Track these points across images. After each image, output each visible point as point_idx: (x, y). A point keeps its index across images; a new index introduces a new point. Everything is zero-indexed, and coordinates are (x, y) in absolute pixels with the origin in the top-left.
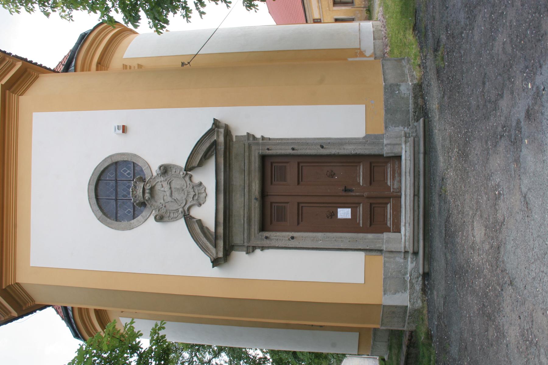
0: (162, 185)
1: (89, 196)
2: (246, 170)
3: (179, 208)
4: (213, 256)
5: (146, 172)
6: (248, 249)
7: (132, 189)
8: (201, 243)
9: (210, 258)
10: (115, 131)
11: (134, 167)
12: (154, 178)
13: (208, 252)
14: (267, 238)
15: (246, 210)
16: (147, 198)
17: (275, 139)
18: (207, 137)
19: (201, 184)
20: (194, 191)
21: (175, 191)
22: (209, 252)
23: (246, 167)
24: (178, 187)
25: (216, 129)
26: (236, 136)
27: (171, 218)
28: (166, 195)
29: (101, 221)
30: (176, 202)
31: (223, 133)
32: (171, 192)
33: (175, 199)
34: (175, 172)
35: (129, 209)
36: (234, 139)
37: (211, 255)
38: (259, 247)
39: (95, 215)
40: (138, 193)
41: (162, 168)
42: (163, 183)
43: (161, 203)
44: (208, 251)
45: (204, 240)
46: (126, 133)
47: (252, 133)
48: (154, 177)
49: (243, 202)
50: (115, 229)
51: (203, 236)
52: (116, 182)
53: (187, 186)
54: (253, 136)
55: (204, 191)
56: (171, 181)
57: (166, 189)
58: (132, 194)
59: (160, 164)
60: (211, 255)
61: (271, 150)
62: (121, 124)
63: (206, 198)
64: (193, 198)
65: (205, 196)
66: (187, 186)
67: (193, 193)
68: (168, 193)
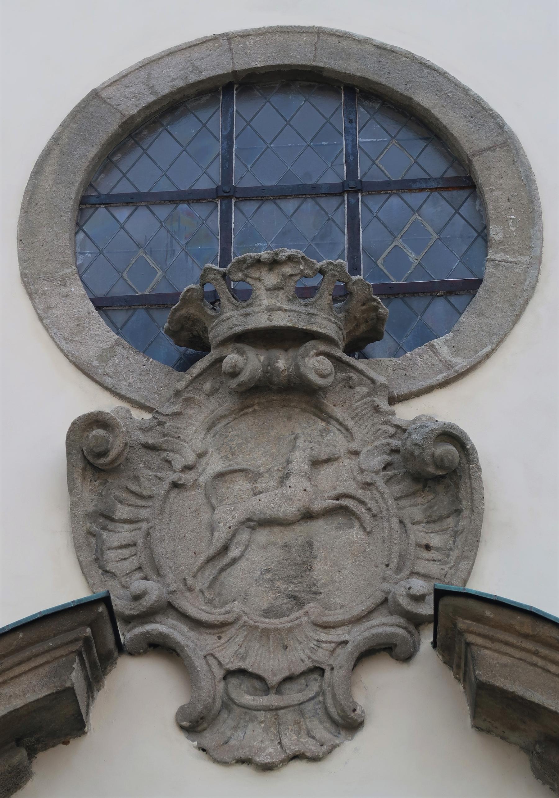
1: (245, 35)
12: (376, 409)
24: (317, 565)
33: (234, 552)
41: (451, 448)
48: (384, 405)
53: (326, 627)
64: (242, 672)
65: (261, 759)
66: (326, 627)
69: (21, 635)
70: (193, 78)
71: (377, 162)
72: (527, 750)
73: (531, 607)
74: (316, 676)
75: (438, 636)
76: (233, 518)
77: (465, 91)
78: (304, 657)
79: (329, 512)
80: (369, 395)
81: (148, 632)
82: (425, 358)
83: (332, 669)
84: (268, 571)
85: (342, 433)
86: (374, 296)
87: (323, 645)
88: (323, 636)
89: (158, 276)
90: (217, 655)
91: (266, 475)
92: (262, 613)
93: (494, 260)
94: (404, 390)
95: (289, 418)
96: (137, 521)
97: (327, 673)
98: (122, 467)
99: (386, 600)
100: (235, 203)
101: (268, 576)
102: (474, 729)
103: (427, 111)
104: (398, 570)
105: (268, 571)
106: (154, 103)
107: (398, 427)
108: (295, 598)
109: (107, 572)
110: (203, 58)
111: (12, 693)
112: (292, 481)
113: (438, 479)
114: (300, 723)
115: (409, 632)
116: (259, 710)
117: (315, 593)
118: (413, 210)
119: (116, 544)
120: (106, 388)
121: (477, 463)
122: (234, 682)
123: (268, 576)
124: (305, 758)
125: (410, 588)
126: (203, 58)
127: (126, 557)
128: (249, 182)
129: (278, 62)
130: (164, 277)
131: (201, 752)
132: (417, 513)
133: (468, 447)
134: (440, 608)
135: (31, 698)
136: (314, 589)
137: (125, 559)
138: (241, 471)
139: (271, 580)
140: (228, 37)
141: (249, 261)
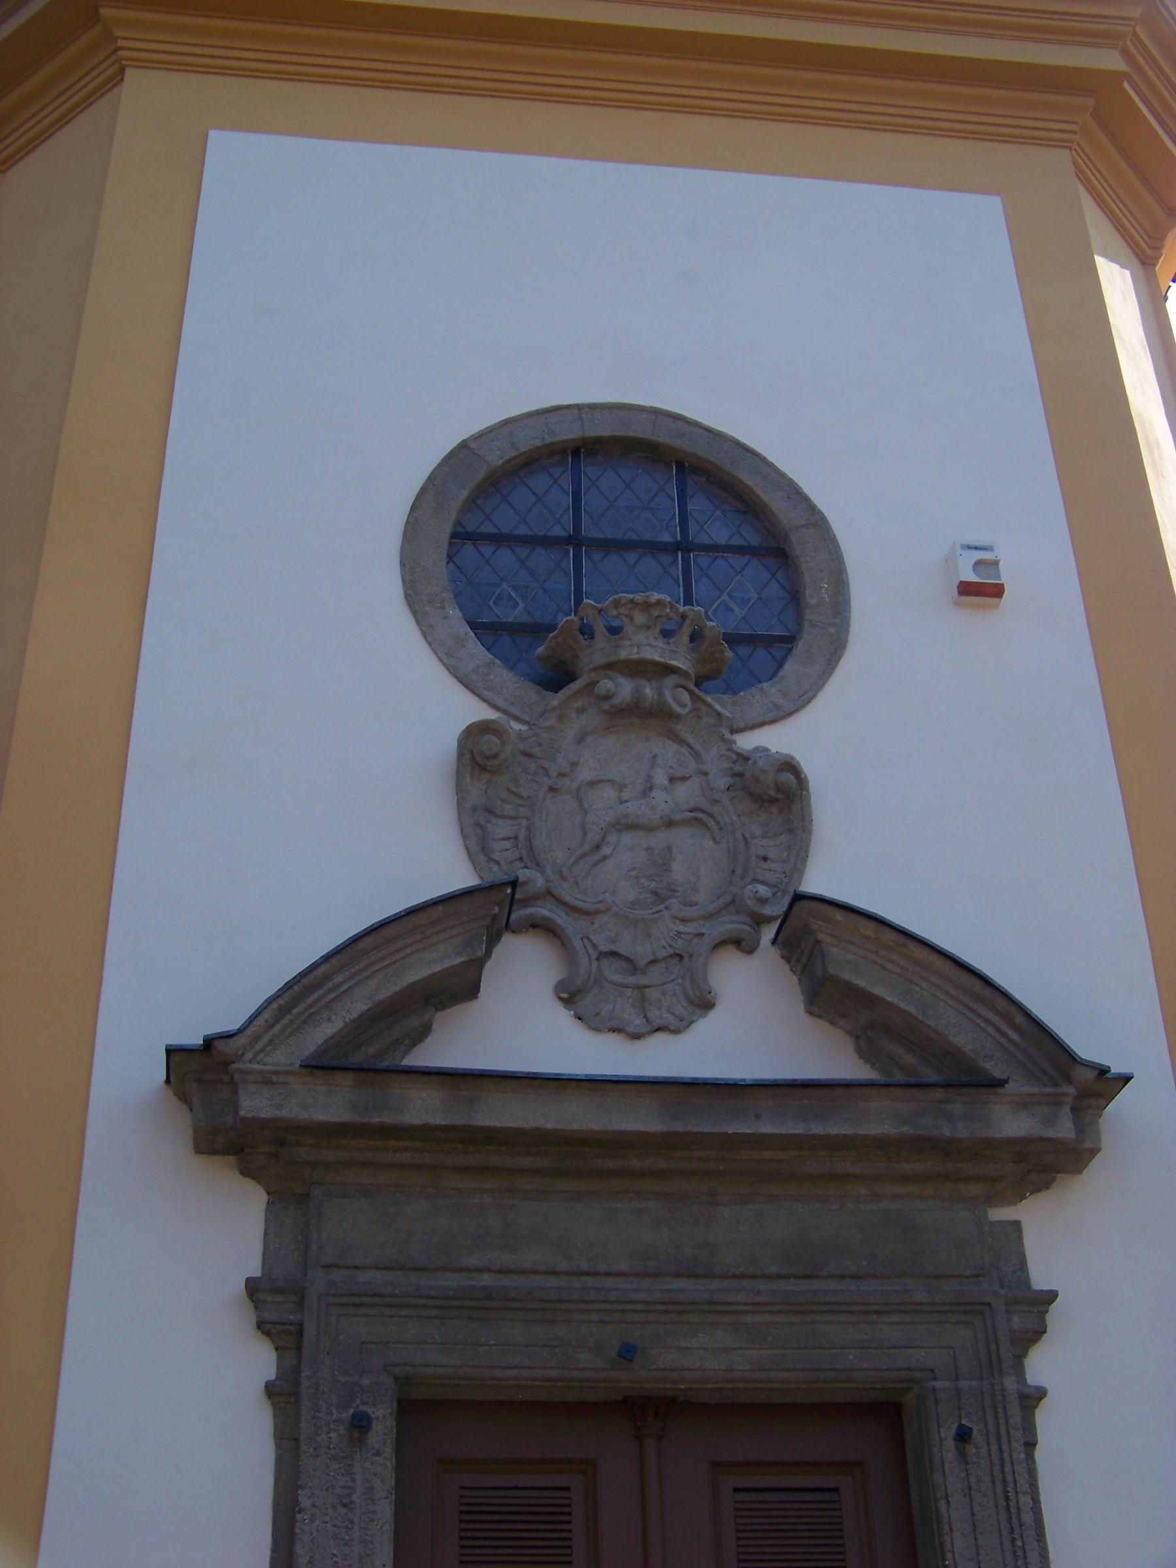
0: (684, 779)
1: (593, 407)
2: (816, 1285)
3: (549, 871)
4: (250, 1055)
5: (756, 699)
6: (281, 1291)
7: (659, 603)
8: (339, 979)
9: (240, 1031)
10: (969, 548)
11: (770, 641)
12: (722, 738)
13: (277, 1019)
14: (360, 1425)
15: (553, 1282)
16: (606, 685)
17: (1036, 1480)
18: (1015, 1037)
19: (705, 1004)
20: (654, 962)
21: (649, 849)
22: (278, 1027)
23: (833, 1284)
24: (676, 867)
25: (1072, 1090)
26: (1017, 1225)
27: (482, 821)
28: (625, 796)
29: (451, 455)
30: (583, 856)
31: (1050, 1133)
32: (647, 829)
33: (606, 850)
34: (765, 859)
35: (521, 605)
36: (1001, 1214)
37: (257, 1038)
38: (297, 1370)
39: (489, 431)
40: (640, 637)
41: (792, 778)
42: (694, 784)
43: (574, 765)
44: (285, 1021)
45: (358, 1005)
46: (956, 603)
47: (1056, 1314)
48: (728, 736)
49: (602, 1267)
50: (408, 523)
51: (386, 993)
52: (673, 549)
53: (684, 920)
54: (1038, 1333)
55: (657, 1023)
56: (708, 828)
57: (659, 796)
58: (632, 601)
59: (809, 769)
60: (257, 1038)
61: (962, 1455)
62: (1006, 578)
63: (614, 1037)
64: (614, 954)
65: (630, 1029)
66: (684, 920)
67: (642, 951)
68: (635, 808)
69: (441, 908)
70: (549, 440)
71: (705, 527)
72: (849, 1032)
73: (876, 914)
74: (678, 958)
75: (781, 934)
76: (604, 821)
77: (782, 475)
78: (665, 944)
79: (685, 822)
80: (715, 726)
81: (532, 914)
82: (757, 698)
83: (691, 956)
84: (634, 868)
85: (692, 756)
86: (722, 641)
87: (683, 936)
88: (682, 928)
89: (520, 606)
90: (591, 937)
91: (630, 786)
92: (629, 905)
93: (811, 620)
94: (741, 725)
95: (648, 739)
96: (518, 818)
97: (686, 960)
98: (504, 770)
99: (733, 901)
100: (585, 550)
101: (634, 873)
102: (807, 1015)
103: (750, 488)
104: (743, 876)
105: (634, 868)
106: (515, 457)
107: (739, 754)
108: (657, 894)
109: (492, 859)
110: (557, 423)
111: (431, 959)
112: (655, 793)
113: (773, 801)
114: (661, 1000)
115: (754, 929)
116: (628, 987)
117: (673, 891)
118: (736, 571)
119: (500, 836)
120: (485, 700)
121: (808, 790)
122: (605, 962)
123: (634, 873)
124: (667, 1031)
125: (757, 892)
126: (557, 423)
127: (509, 848)
128: (595, 534)
129: (622, 433)
130: (525, 608)
131: (578, 1020)
132: (757, 830)
133: (803, 776)
134: (795, 909)
135: (447, 964)
136: (673, 887)
137: (507, 850)
138: (609, 781)
139: (637, 877)
140: (579, 407)
141: (623, 601)
